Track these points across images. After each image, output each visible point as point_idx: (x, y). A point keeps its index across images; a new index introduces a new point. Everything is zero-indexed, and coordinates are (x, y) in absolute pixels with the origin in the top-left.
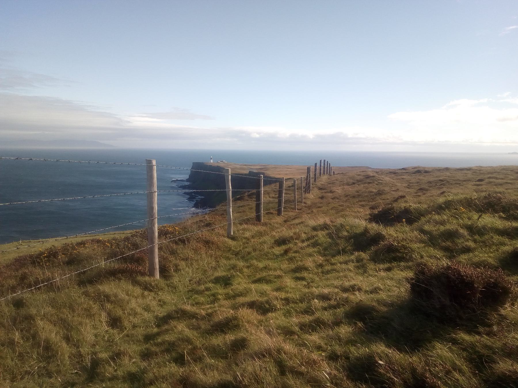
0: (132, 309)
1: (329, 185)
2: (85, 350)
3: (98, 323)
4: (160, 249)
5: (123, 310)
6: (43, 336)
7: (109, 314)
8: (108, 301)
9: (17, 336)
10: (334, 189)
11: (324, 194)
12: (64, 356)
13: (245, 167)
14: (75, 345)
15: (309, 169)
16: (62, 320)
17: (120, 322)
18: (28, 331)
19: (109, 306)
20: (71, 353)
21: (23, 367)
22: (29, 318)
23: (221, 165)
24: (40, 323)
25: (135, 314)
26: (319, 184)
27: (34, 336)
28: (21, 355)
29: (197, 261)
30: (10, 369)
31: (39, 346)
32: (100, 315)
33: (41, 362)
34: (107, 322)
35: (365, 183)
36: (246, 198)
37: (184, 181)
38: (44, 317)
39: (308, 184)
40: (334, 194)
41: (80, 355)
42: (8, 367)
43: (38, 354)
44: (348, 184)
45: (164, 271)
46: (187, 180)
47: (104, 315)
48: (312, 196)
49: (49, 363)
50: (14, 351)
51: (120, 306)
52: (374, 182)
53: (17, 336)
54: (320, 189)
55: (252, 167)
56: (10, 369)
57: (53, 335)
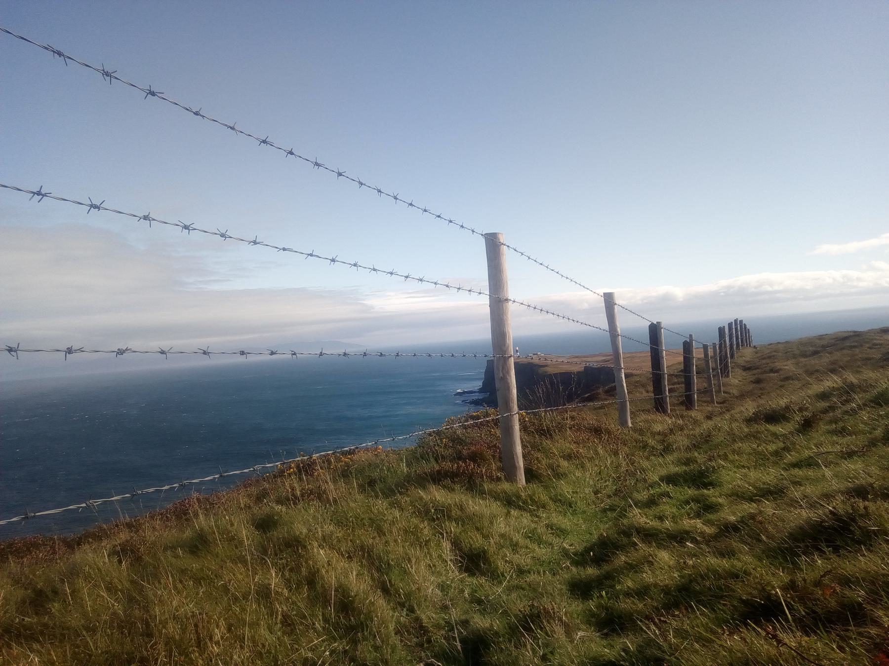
0: (502, 536)
1: (764, 361)
2: (428, 616)
3: (439, 564)
4: (524, 428)
5: (486, 537)
6: (331, 579)
7: (456, 544)
8: (450, 518)
9: (274, 580)
10: (778, 365)
11: (761, 377)
12: (387, 627)
13: (576, 360)
14: (402, 605)
15: (721, 330)
16: (362, 548)
17: (487, 561)
18: (295, 570)
19: (453, 527)
20: (398, 622)
21: (297, 650)
22: (294, 544)
23: (536, 360)
24: (321, 554)
25: (515, 547)
26: (741, 361)
27: (312, 580)
28: (287, 622)
29: (591, 459)
30: (269, 652)
31: (326, 602)
32: (439, 545)
33: (335, 640)
34: (455, 562)
35: (843, 349)
36: (603, 396)
37: (475, 392)
38: (326, 541)
39: (723, 359)
40: (781, 372)
41: (422, 629)
42: (264, 646)
43: (326, 620)
44: (804, 355)
45: (531, 475)
46: (481, 391)
47: (446, 545)
48: (736, 380)
49: (354, 642)
50: (272, 613)
51: (477, 529)
52: (862, 346)
53: (274, 580)
54: (746, 369)
55: (589, 359)
56: (269, 652)
57: (353, 576)
